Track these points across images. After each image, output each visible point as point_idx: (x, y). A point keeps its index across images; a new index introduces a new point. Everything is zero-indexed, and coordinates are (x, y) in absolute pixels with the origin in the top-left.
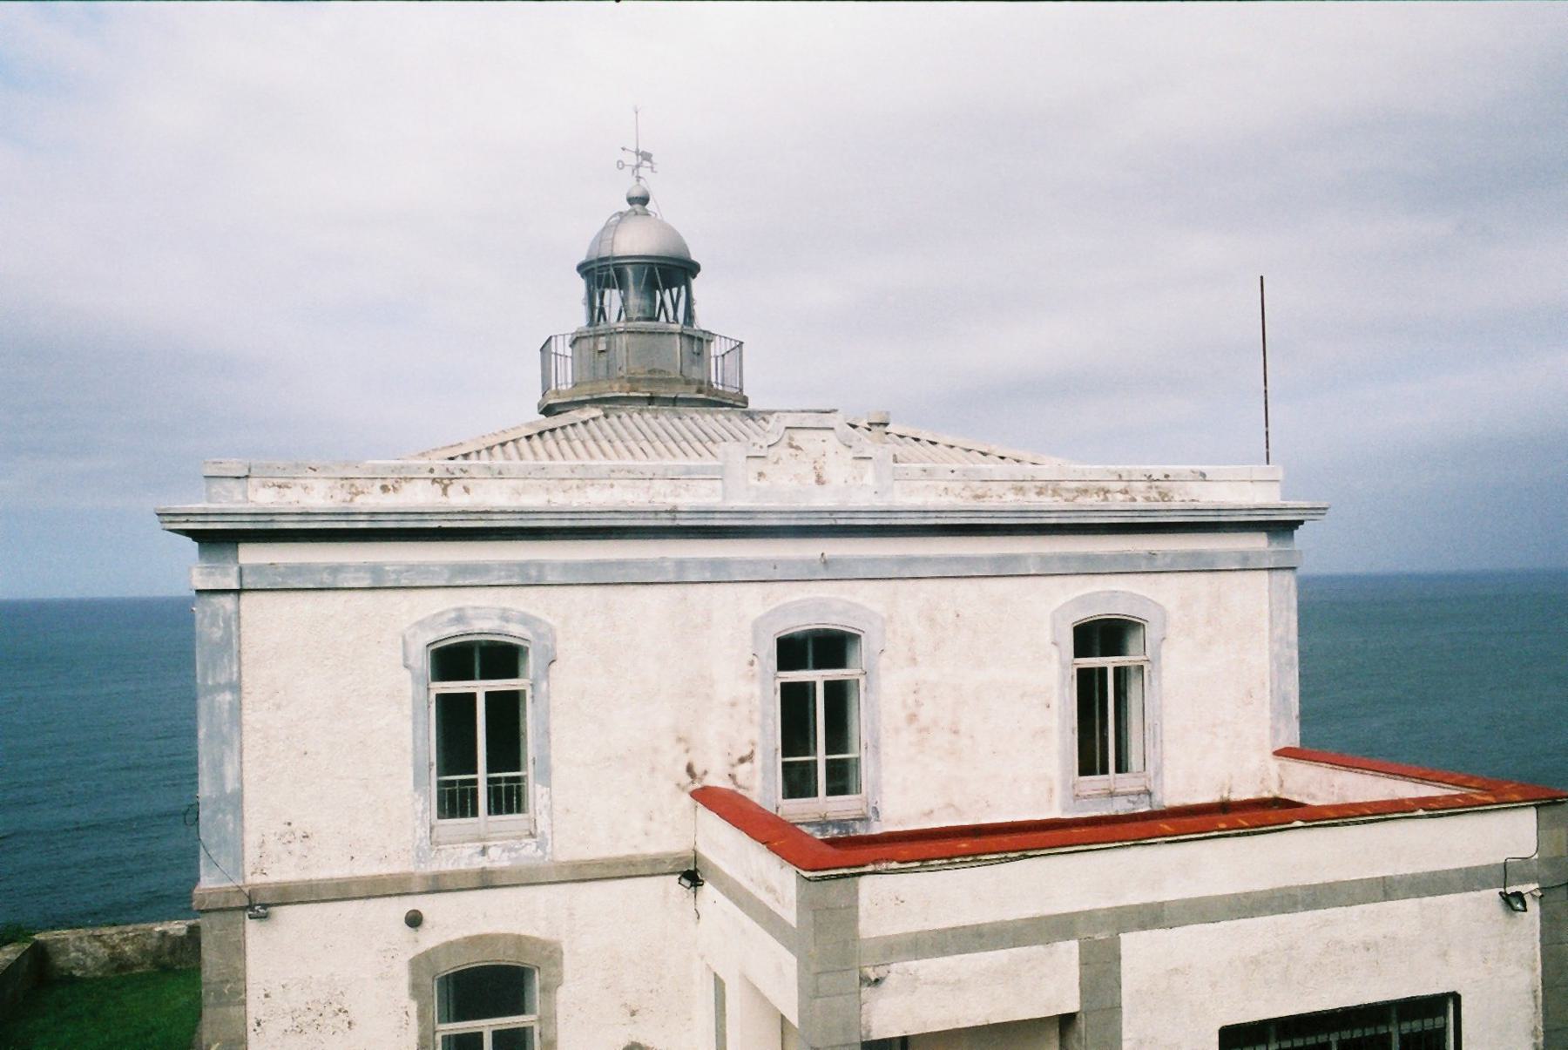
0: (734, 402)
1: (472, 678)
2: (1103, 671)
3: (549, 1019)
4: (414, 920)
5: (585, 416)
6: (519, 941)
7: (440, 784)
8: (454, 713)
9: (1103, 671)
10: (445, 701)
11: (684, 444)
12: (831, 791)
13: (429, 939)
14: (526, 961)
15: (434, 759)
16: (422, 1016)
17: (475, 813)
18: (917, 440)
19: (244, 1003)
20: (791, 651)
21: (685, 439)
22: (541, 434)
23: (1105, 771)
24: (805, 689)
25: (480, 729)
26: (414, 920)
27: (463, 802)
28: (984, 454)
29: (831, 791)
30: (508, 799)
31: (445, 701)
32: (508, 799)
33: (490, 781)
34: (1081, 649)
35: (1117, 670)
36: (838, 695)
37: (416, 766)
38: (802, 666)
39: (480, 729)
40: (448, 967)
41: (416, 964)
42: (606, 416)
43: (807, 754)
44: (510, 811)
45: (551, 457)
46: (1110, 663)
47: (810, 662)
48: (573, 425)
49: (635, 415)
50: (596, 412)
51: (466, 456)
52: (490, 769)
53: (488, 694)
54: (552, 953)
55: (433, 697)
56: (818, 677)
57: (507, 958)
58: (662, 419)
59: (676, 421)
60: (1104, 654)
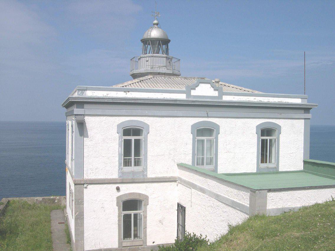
0: (131, 75)
1: (130, 136)
2: (267, 140)
3: (145, 212)
4: (118, 189)
5: (149, 77)
6: (140, 194)
7: (124, 159)
8: (127, 144)
9: (267, 140)
10: (125, 141)
11: (173, 85)
12: (135, 165)
13: (121, 193)
14: (141, 199)
15: (123, 153)
16: (119, 209)
17: (131, 166)
18: (225, 85)
19: (83, 204)
20: (127, 132)
21: (155, 82)
22: (140, 81)
23: (266, 162)
24: (130, 141)
25: (132, 146)
26: (118, 189)
27: (128, 163)
28: (233, 87)
29: (135, 165)
30: (137, 163)
31: (125, 141)
32: (137, 163)
33: (135, 159)
34: (262, 135)
35: (271, 140)
36: (137, 142)
37: (119, 154)
38: (129, 135)
39: (132, 146)
40: (125, 199)
41: (118, 198)
42: (154, 78)
43: (130, 157)
44: (128, 166)
45: (153, 87)
46: (268, 138)
47: (132, 134)
48: (147, 79)
49: (160, 78)
50: (151, 77)
51: (126, 86)
52: (135, 156)
53: (135, 140)
54: (147, 198)
55: (123, 140)
56: (133, 138)
57: (137, 198)
58: (166, 78)
59: (169, 79)
60: (267, 136)
